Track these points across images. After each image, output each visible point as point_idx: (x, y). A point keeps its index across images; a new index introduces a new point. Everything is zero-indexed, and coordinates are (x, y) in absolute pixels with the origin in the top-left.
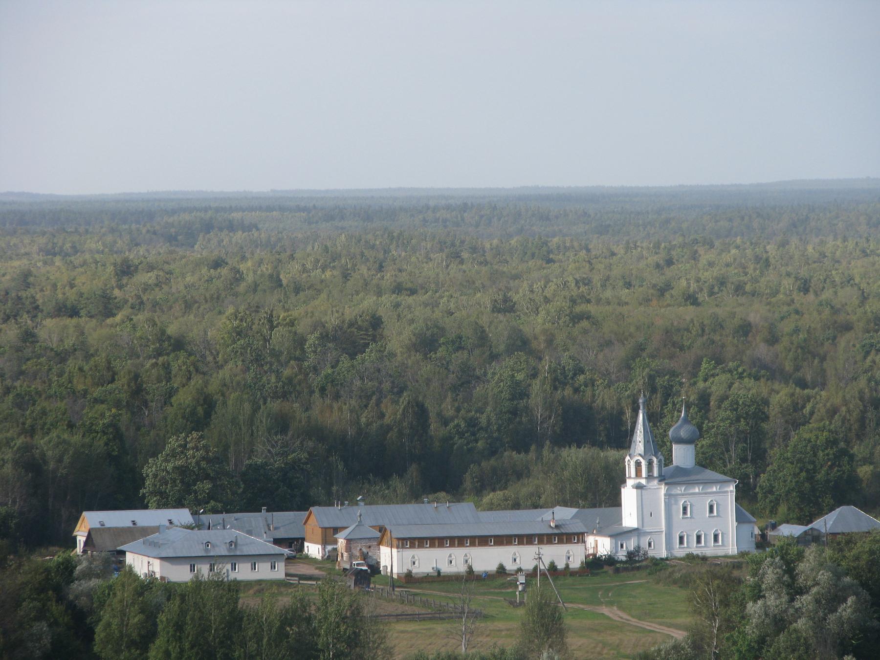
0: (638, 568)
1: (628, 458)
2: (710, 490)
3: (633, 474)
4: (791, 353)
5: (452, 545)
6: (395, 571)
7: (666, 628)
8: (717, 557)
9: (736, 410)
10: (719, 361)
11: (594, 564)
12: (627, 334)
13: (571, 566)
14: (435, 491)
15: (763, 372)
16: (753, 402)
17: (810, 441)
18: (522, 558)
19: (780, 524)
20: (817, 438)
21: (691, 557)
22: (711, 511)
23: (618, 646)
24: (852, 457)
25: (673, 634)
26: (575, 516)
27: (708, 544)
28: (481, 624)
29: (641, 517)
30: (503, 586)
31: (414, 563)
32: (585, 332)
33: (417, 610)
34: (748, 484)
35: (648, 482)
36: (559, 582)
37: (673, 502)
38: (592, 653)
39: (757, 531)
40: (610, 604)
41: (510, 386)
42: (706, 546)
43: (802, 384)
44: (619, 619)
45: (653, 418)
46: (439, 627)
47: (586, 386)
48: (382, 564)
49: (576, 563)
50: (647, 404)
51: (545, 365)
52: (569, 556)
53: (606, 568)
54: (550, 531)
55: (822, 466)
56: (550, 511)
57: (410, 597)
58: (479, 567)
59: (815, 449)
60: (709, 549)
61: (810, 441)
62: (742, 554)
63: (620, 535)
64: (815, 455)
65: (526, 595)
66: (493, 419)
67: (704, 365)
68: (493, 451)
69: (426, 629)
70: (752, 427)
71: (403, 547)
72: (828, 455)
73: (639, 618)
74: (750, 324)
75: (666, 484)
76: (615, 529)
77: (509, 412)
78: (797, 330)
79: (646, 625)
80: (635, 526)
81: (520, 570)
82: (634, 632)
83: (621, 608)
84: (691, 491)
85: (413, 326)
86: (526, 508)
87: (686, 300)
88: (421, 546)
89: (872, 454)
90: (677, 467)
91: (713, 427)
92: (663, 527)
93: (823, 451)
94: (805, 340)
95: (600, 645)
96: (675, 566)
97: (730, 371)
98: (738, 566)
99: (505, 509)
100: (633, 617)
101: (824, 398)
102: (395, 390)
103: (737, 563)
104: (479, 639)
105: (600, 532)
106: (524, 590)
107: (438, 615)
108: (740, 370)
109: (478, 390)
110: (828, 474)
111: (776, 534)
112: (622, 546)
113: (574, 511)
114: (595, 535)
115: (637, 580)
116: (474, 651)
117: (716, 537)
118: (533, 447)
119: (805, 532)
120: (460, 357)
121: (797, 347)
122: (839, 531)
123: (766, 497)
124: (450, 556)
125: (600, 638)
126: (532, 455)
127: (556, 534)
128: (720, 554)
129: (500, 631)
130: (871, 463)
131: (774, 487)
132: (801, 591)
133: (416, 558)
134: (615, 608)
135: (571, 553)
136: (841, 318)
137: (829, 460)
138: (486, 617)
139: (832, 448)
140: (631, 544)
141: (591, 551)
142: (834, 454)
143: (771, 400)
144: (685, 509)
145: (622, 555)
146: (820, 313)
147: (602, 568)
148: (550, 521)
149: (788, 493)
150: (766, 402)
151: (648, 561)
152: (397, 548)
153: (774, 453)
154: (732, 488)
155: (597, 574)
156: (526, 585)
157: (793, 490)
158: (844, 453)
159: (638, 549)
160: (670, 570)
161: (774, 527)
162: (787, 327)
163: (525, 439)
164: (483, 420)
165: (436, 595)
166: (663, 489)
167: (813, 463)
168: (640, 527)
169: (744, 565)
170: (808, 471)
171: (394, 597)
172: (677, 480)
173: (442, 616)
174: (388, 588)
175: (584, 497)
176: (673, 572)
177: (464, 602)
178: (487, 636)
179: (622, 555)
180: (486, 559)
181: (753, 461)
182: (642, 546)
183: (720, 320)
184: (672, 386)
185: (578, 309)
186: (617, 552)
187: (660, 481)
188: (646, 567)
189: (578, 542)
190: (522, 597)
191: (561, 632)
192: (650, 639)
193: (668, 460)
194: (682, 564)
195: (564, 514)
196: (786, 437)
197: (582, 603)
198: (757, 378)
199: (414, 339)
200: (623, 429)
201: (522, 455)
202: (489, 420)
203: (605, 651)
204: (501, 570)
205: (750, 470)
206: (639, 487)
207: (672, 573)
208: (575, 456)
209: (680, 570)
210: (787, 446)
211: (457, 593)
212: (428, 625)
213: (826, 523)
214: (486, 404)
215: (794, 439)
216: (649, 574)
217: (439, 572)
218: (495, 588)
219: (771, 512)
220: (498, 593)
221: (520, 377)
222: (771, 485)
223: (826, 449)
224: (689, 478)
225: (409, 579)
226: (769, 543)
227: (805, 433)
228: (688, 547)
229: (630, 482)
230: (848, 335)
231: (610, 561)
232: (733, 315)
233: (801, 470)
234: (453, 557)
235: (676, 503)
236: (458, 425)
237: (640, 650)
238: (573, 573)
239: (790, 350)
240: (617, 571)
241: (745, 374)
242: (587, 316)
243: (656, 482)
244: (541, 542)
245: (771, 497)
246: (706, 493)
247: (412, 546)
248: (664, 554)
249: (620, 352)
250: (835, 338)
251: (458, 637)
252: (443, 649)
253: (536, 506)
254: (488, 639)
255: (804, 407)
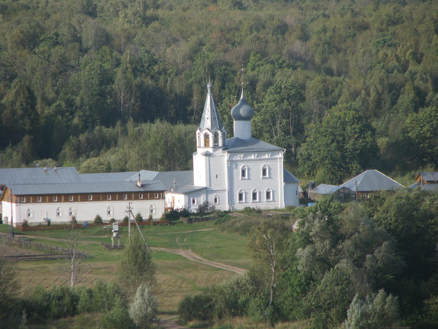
0: (207, 219)
1: (198, 131)
2: (263, 157)
3: (202, 144)
4: (319, 48)
5: (59, 201)
6: (14, 221)
7: (231, 267)
8: (269, 211)
9: (279, 93)
10: (264, 54)
11: (172, 216)
12: (189, 32)
13: (154, 217)
14: (41, 158)
15: (299, 63)
16: (293, 86)
17: (340, 118)
18: (116, 211)
19: (318, 185)
20: (345, 114)
21: (248, 210)
22: (264, 173)
23: (194, 281)
24: (374, 131)
25: (236, 272)
26: (156, 178)
27: (248, 201)
28: (87, 264)
29: (210, 179)
30: (100, 233)
31: (29, 215)
32: (157, 31)
33: (33, 252)
34: (291, 152)
35: (214, 151)
36: (145, 230)
37: (234, 166)
38: (174, 286)
39: (300, 190)
40: (186, 247)
41: (99, 74)
42: (260, 201)
43: (330, 72)
44: (192, 259)
45: (218, 101)
46: (51, 266)
47: (160, 74)
48: (4, 216)
49: (158, 215)
50: (212, 89)
51: (125, 58)
52: (143, 208)
53: (181, 219)
54: (137, 190)
55: (350, 137)
56: (137, 174)
57: (26, 242)
58: (81, 218)
59: (344, 124)
60: (263, 204)
61: (340, 118)
62: (290, 208)
63: (192, 193)
64: (344, 129)
65: (119, 240)
66: (86, 100)
67: (252, 58)
68: (87, 125)
69: (40, 268)
70: (293, 106)
71: (20, 202)
72: (354, 129)
73: (210, 259)
74: (286, 25)
75: (228, 152)
76: (188, 188)
77: (98, 94)
78: (325, 30)
79: (215, 264)
80: (204, 186)
81: (113, 221)
82: (206, 270)
83: (194, 251)
84: (249, 158)
85: (19, 27)
86: (115, 171)
87: (234, 6)
88: (35, 201)
89: (387, 128)
90: (237, 139)
91: (263, 107)
92: (226, 186)
93: (351, 126)
94: (331, 37)
95: (180, 280)
96: (236, 217)
97: (272, 62)
98: (286, 217)
99: (99, 172)
100: (204, 258)
101: (353, 82)
102: (8, 77)
103: (286, 216)
104: (84, 276)
105: (176, 191)
106: (117, 236)
107: (50, 256)
108: (280, 61)
109: (73, 76)
110: (355, 144)
111: (315, 192)
112: (194, 202)
113: (156, 173)
114: (173, 192)
115: (206, 228)
116: (80, 285)
117: (268, 194)
118: (118, 123)
119: (338, 191)
120: (58, 50)
121: (324, 44)
122: (370, 190)
123: (305, 163)
124: (58, 209)
125: (179, 275)
126: (118, 128)
127: (141, 192)
128: (271, 208)
129: (100, 269)
130: (387, 136)
131: (311, 155)
132: (342, 238)
133: (31, 211)
134: (190, 251)
135: (154, 207)
136: (359, 19)
137: (356, 133)
138: (92, 258)
139: (357, 123)
140: (201, 200)
141: (169, 206)
142: (359, 128)
143: (307, 85)
144: (243, 172)
145: (194, 209)
146: (342, 16)
147: (179, 219)
148: (137, 182)
149: (322, 160)
150: (303, 87)
151: (215, 213)
152: (16, 202)
153: (311, 128)
154: (281, 155)
155: (174, 224)
156: (119, 232)
157: (326, 157)
158: (368, 127)
159: (206, 204)
160: (233, 220)
161: (314, 186)
162: (316, 27)
163: (111, 116)
164: (78, 100)
165: (48, 241)
166: (226, 156)
167: (343, 135)
168: (208, 187)
169: (290, 217)
170: (338, 142)
171: (14, 242)
172: (237, 149)
173: (52, 257)
174: (10, 235)
175: (162, 162)
176: (235, 222)
177: (73, 246)
178: (89, 273)
179: (194, 209)
180: (86, 212)
181: (294, 134)
182: (209, 201)
183: (263, 21)
184: (227, 74)
185: (150, 12)
186: (189, 207)
187: (224, 150)
188: (214, 218)
189: (159, 198)
190: (116, 242)
191: (152, 269)
192: (219, 276)
193: (231, 132)
194: (241, 216)
195: (148, 176)
196: (321, 116)
197: (164, 247)
198: (295, 68)
199: (22, 36)
200: (189, 109)
201: (110, 129)
202: (82, 100)
203: (184, 285)
204: (99, 220)
205: (293, 140)
206: (207, 155)
207: (234, 223)
208: (156, 128)
209: (240, 221)
210: (321, 122)
211: (66, 239)
212: (42, 264)
213: (353, 183)
214: (79, 88)
215: (327, 117)
216: (216, 224)
217: (49, 222)
218: (94, 235)
219: (309, 174)
220: (96, 239)
221: (107, 66)
222: (309, 153)
223: (353, 124)
224: (247, 148)
225: (25, 227)
226: (310, 199)
227: (335, 111)
228: (246, 202)
229: (200, 151)
230: (366, 33)
231: (185, 213)
232: (272, 17)
233: (333, 141)
234: (60, 210)
235: (237, 167)
236: (60, 105)
237: (210, 284)
238: (156, 223)
239: (318, 45)
240: (190, 221)
241: (284, 65)
242: (155, 18)
243: (220, 151)
244: (130, 198)
245: (310, 163)
246: (260, 160)
247: (28, 202)
248: (227, 208)
249: (184, 47)
250: (354, 35)
251: (67, 274)
252: (56, 283)
253: (123, 170)
254: (91, 275)
255: (333, 91)
